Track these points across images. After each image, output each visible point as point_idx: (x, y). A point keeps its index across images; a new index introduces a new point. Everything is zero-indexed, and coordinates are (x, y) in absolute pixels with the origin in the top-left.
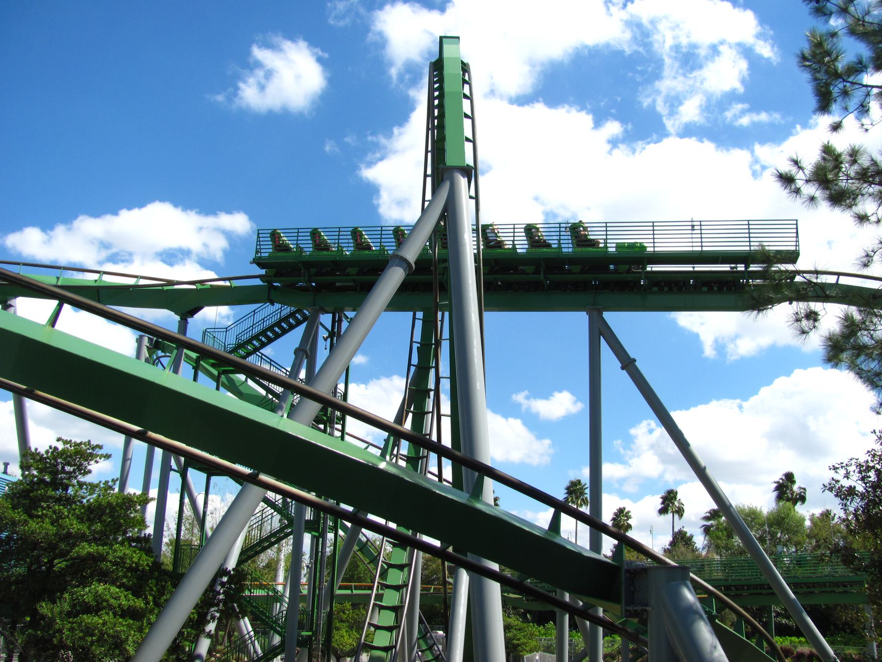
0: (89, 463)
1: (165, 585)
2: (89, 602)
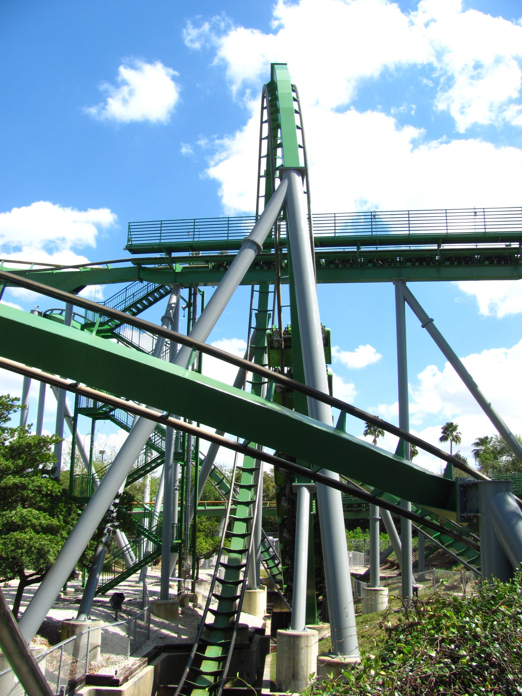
0: (9, 412)
1: (71, 507)
2: (16, 522)
